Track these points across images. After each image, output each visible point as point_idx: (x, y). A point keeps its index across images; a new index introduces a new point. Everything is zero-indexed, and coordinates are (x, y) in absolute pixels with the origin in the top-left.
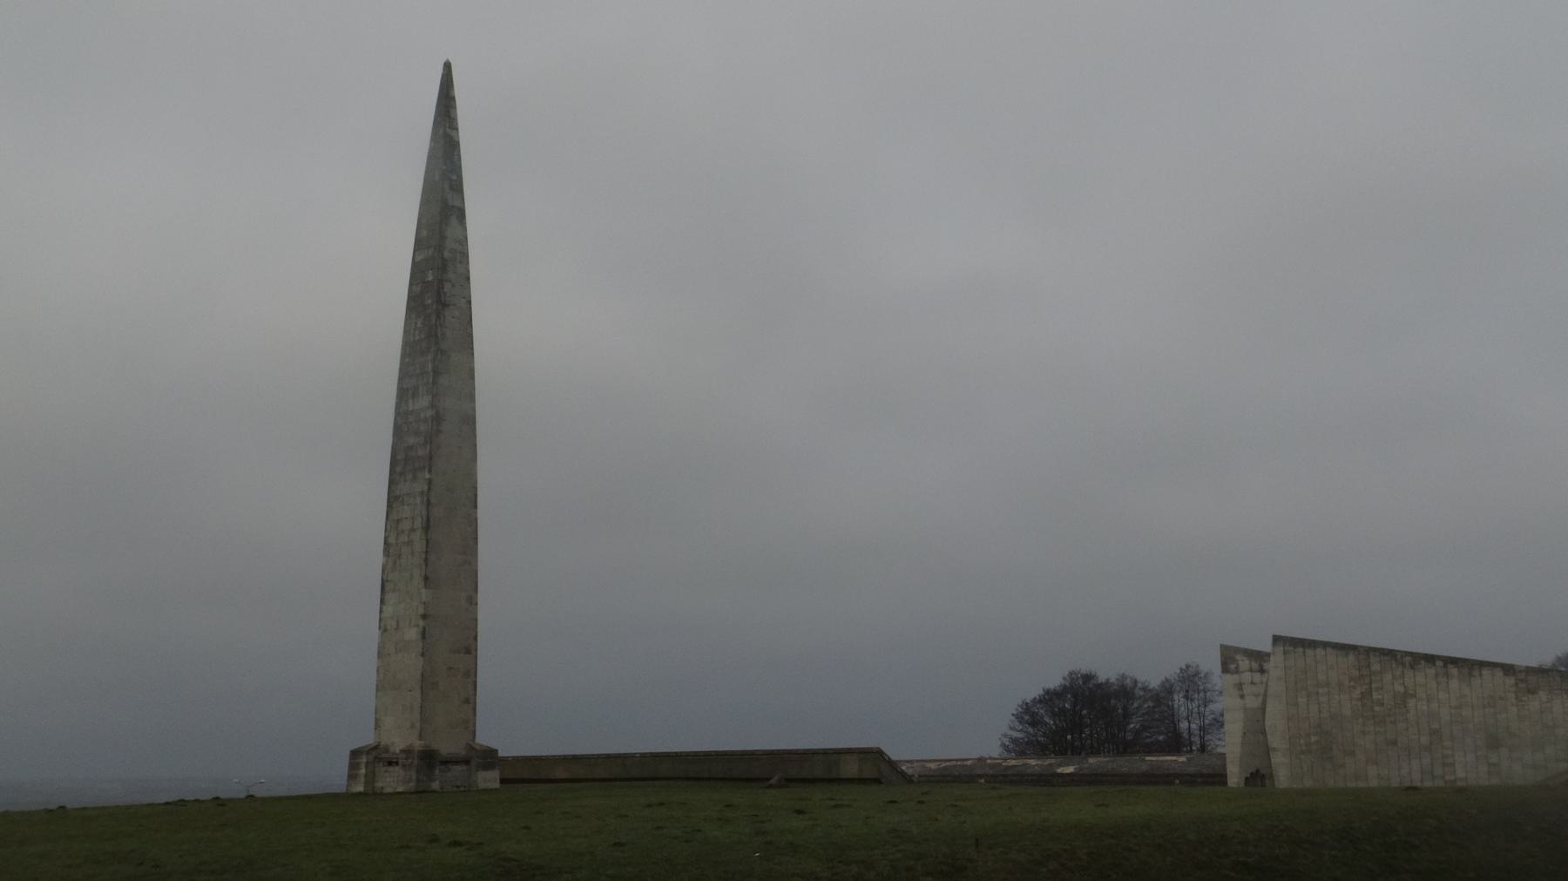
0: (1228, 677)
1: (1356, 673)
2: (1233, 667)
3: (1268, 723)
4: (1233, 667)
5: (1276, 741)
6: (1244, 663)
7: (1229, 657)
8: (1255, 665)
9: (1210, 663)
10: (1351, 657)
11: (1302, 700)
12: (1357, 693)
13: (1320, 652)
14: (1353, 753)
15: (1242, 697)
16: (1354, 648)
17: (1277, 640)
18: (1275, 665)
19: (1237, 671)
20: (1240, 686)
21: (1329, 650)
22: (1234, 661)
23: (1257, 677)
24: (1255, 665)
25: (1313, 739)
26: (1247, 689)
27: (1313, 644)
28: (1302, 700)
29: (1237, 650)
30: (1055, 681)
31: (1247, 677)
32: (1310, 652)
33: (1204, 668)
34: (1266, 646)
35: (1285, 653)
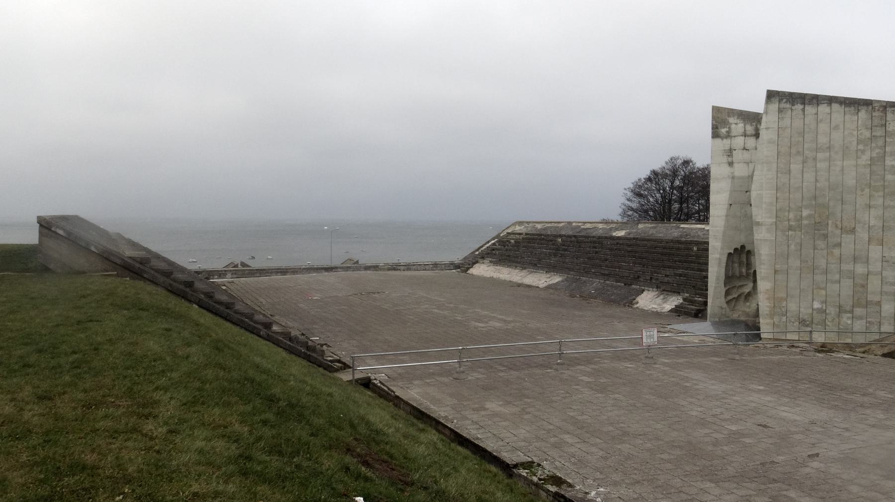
0: (718, 141)
1: (867, 134)
2: (724, 131)
3: (754, 194)
4: (724, 131)
5: (761, 214)
6: (738, 127)
7: (721, 120)
8: (750, 129)
9: (700, 150)
10: (863, 114)
11: (796, 167)
12: (865, 159)
13: (824, 109)
14: (853, 231)
15: (731, 164)
16: (867, 103)
17: (772, 95)
18: (769, 123)
19: (728, 136)
20: (730, 152)
21: (835, 106)
22: (725, 123)
23: (751, 142)
24: (750, 129)
25: (805, 213)
26: (738, 155)
27: (815, 100)
28: (796, 167)
29: (731, 112)
30: (659, 163)
31: (739, 142)
32: (810, 110)
33: (700, 161)
34: (757, 105)
35: (780, 111)
